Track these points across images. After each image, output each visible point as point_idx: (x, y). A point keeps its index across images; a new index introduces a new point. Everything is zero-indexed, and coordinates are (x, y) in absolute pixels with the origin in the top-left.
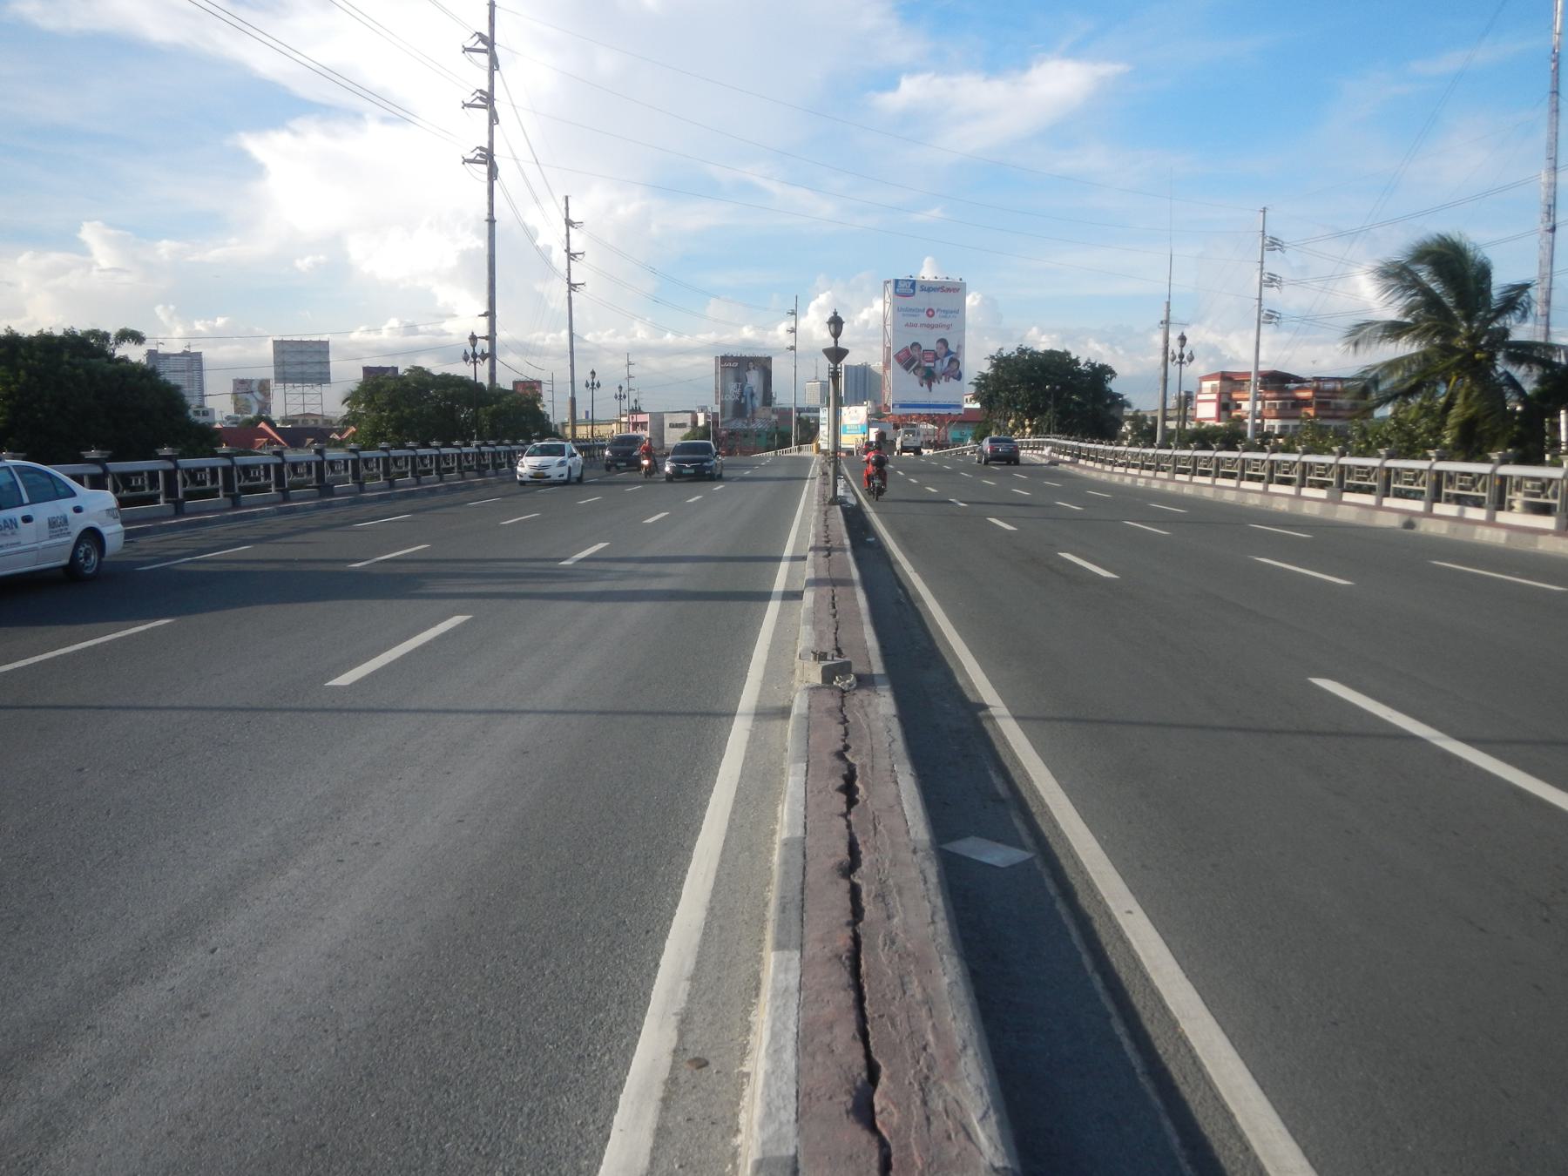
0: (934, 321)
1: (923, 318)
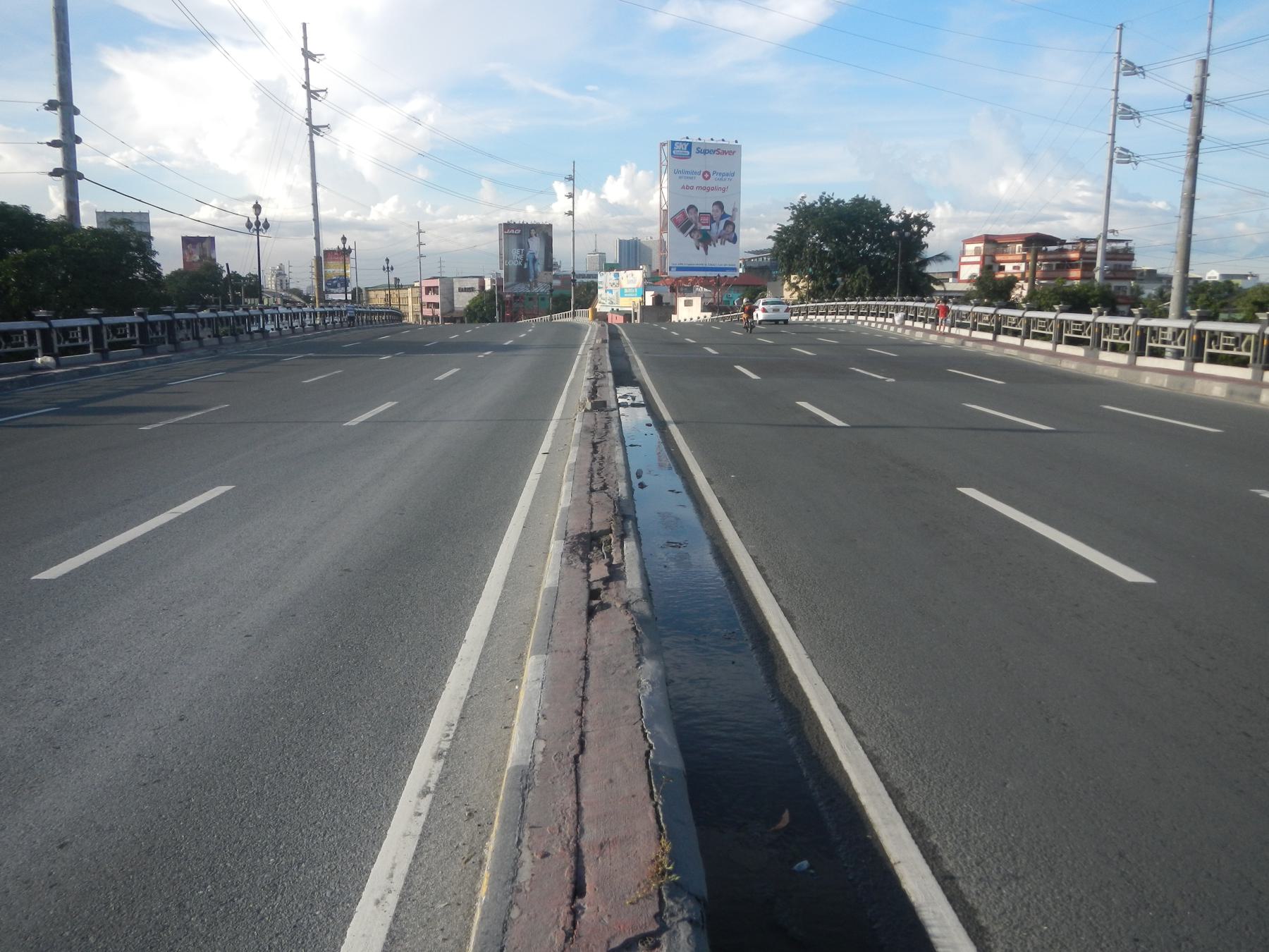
0: (711, 183)
1: (699, 181)
